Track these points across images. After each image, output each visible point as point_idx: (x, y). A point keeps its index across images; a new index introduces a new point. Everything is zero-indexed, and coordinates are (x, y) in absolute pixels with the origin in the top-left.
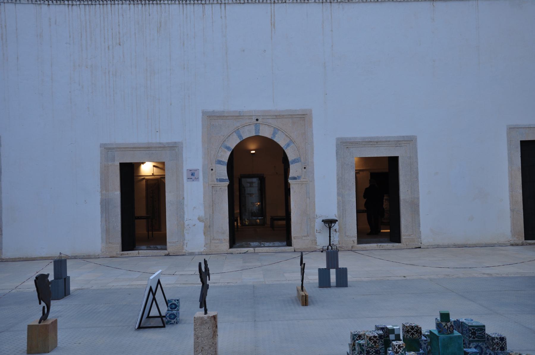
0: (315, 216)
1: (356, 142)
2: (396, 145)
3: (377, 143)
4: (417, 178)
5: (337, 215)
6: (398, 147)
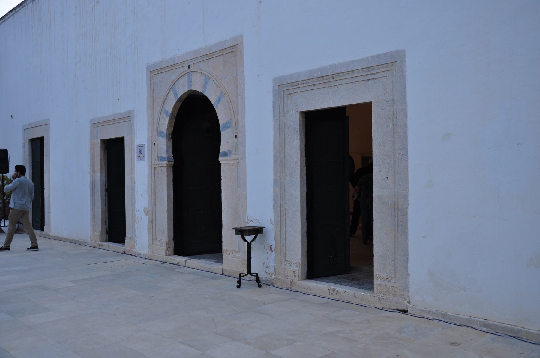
0: (246, 219)
1: (300, 83)
2: (367, 78)
3: (333, 78)
4: (405, 148)
5: (273, 219)
6: (370, 82)
